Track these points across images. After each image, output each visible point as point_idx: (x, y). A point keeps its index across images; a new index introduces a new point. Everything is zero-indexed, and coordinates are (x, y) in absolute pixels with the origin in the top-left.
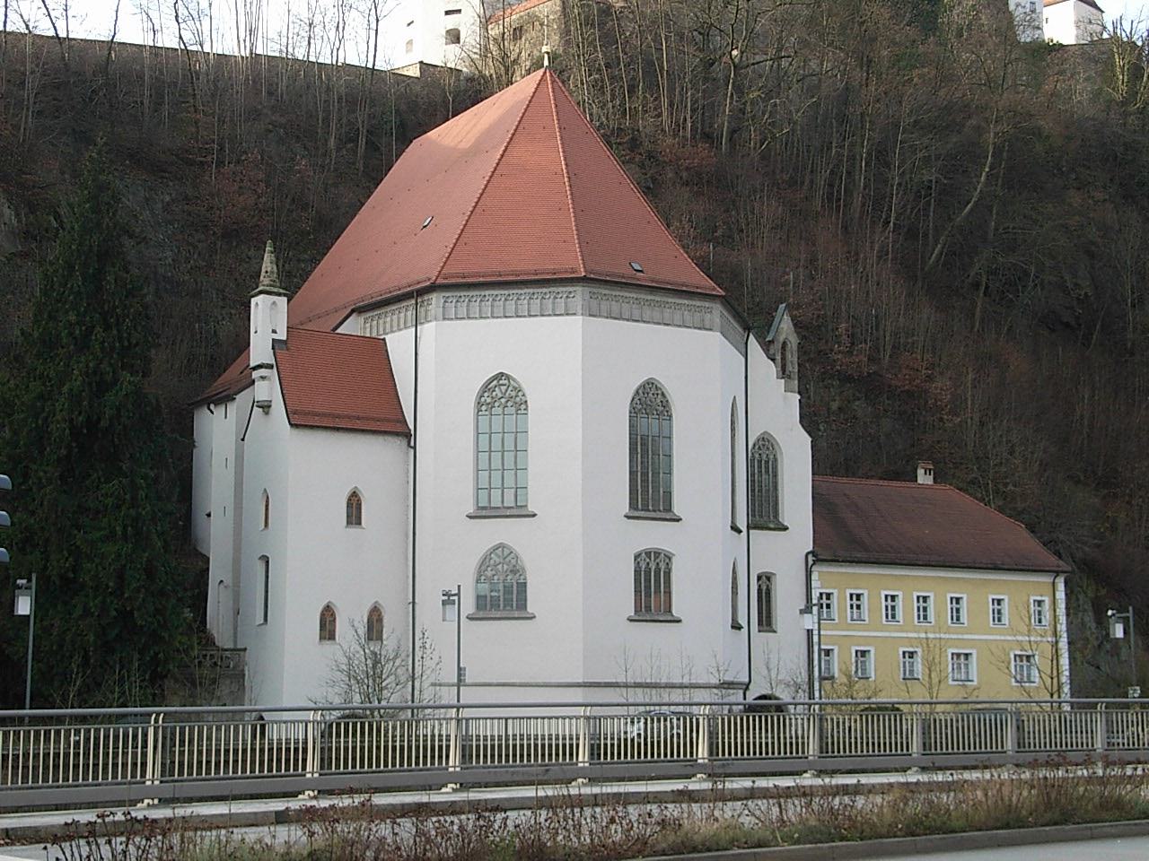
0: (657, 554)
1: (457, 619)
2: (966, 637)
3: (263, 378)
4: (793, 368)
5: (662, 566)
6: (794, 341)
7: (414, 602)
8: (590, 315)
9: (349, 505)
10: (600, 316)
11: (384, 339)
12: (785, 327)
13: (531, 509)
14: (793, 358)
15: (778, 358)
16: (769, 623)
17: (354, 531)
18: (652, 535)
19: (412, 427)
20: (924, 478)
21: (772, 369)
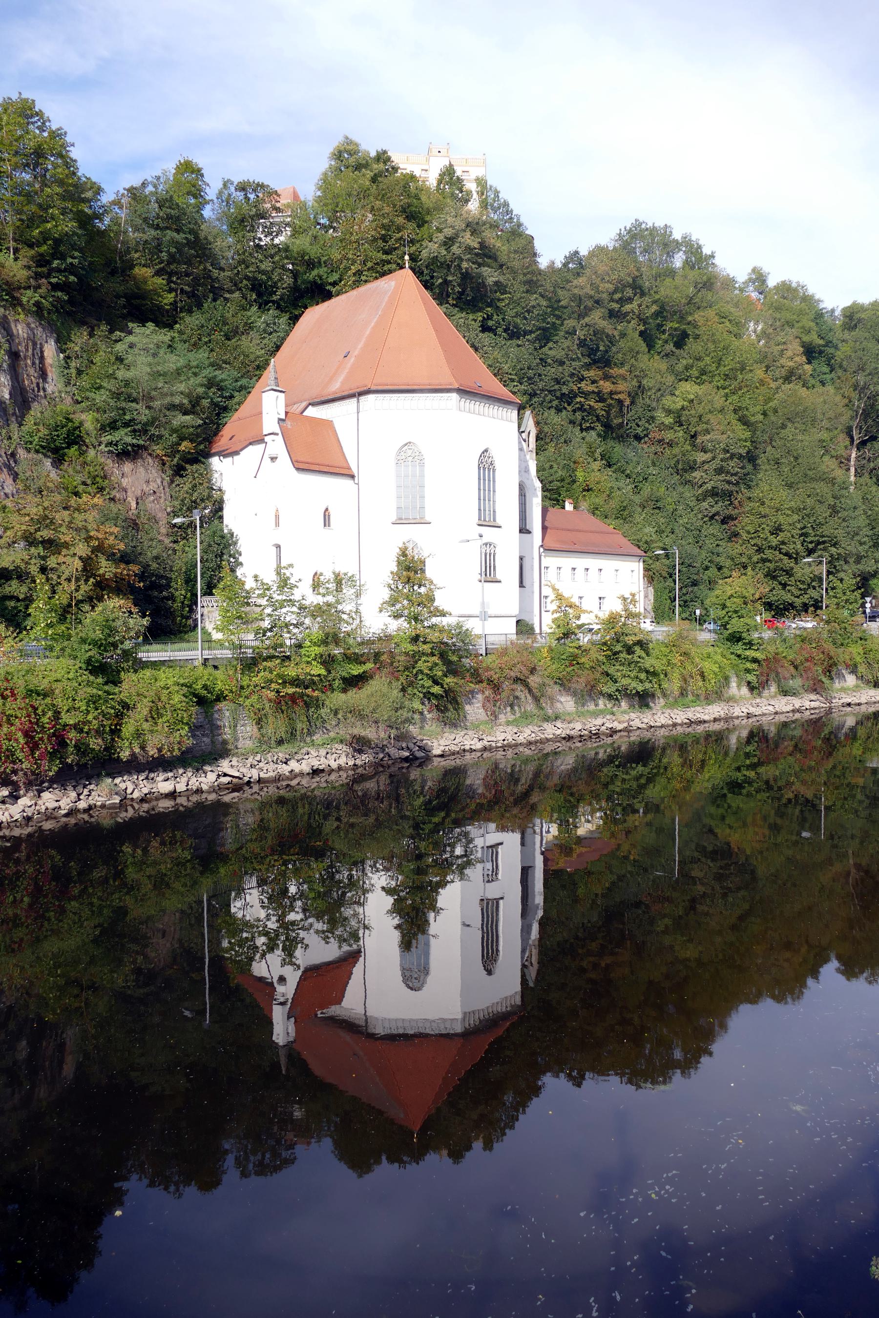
18: (489, 534)
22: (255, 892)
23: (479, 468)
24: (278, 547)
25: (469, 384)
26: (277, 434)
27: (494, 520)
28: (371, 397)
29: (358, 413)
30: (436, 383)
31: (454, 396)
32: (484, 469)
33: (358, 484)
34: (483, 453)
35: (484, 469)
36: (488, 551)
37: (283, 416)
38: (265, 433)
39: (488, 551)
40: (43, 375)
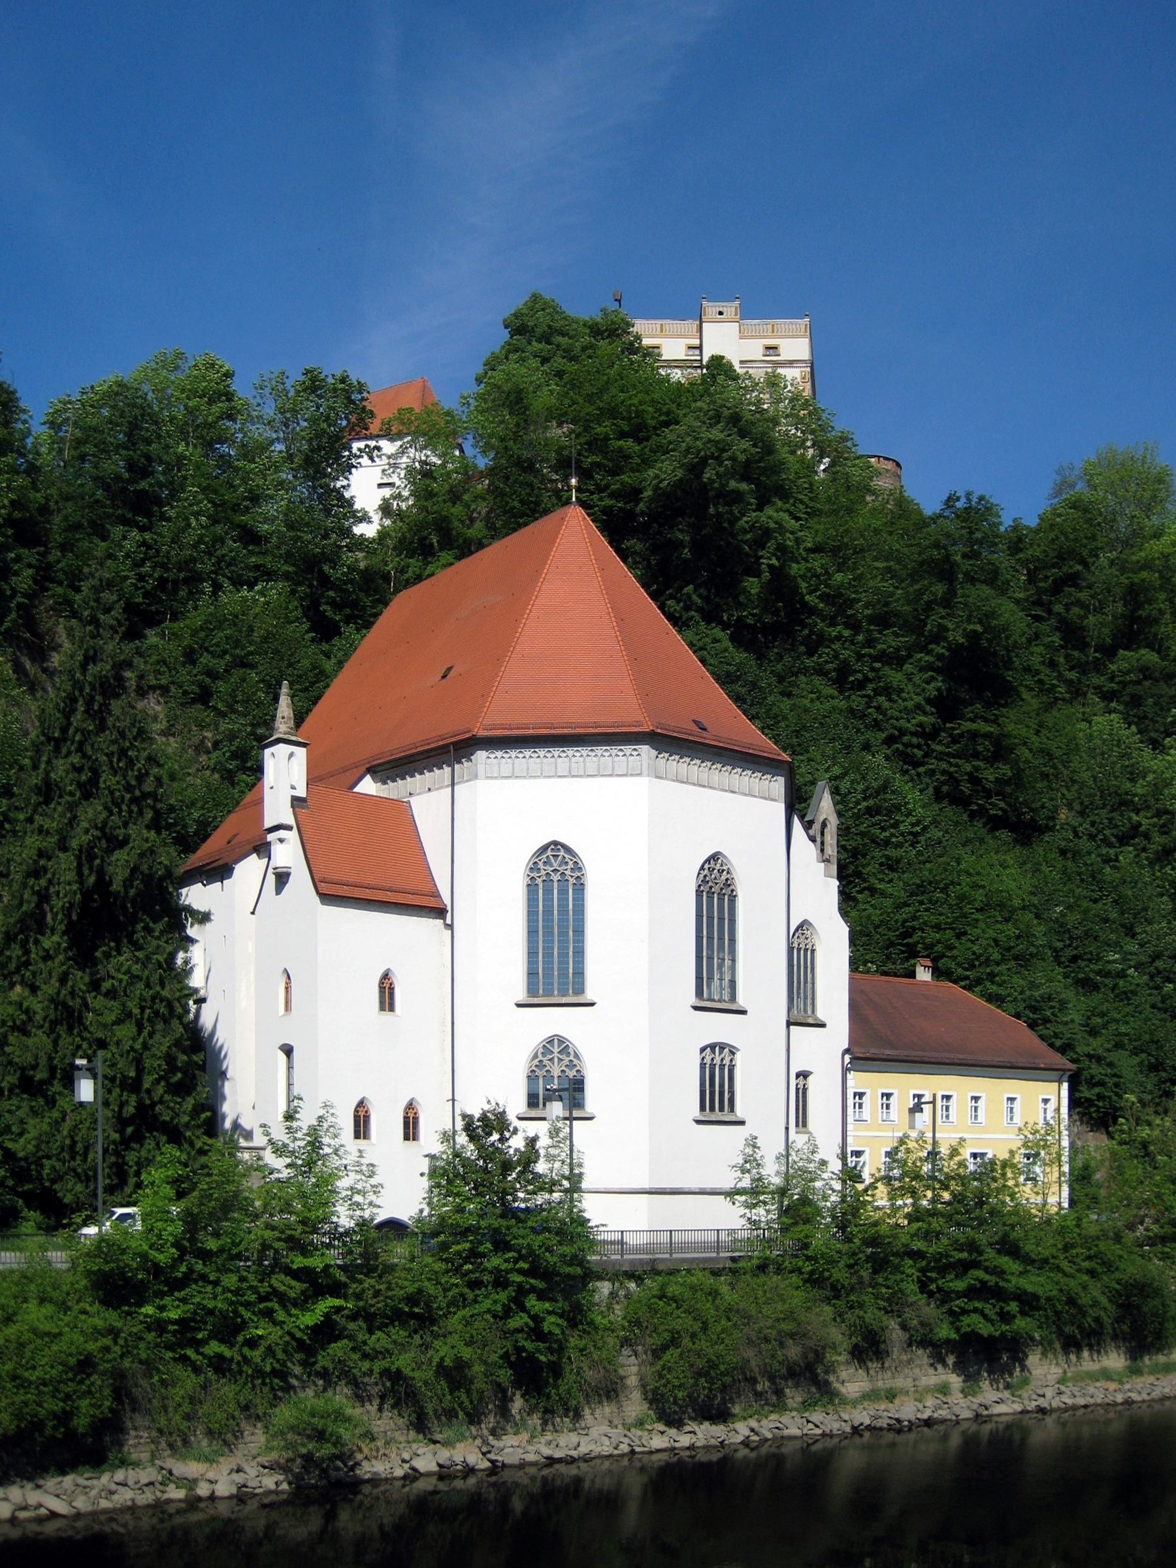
0: (723, 1046)
1: (850, 1127)
2: (984, 1136)
3: (281, 841)
4: (831, 850)
5: (727, 1062)
6: (833, 821)
7: (453, 1100)
8: (657, 777)
9: (382, 989)
10: (666, 778)
11: (409, 802)
12: (825, 807)
13: (589, 995)
14: (831, 838)
15: (819, 839)
16: (805, 1125)
17: (387, 1016)
18: (718, 1027)
19: (447, 901)
20: (924, 975)
21: (811, 850)
22: (49, 1254)
23: (699, 893)
24: (288, 1051)
25: (679, 723)
26: (289, 828)
27: (733, 998)
28: (481, 756)
29: (453, 784)
30: (608, 720)
31: (645, 749)
32: (710, 895)
33: (450, 927)
34: (708, 860)
35: (710, 895)
36: (717, 1061)
37: (302, 792)
38: (268, 823)
39: (717, 1061)
40: (87, 1479)
